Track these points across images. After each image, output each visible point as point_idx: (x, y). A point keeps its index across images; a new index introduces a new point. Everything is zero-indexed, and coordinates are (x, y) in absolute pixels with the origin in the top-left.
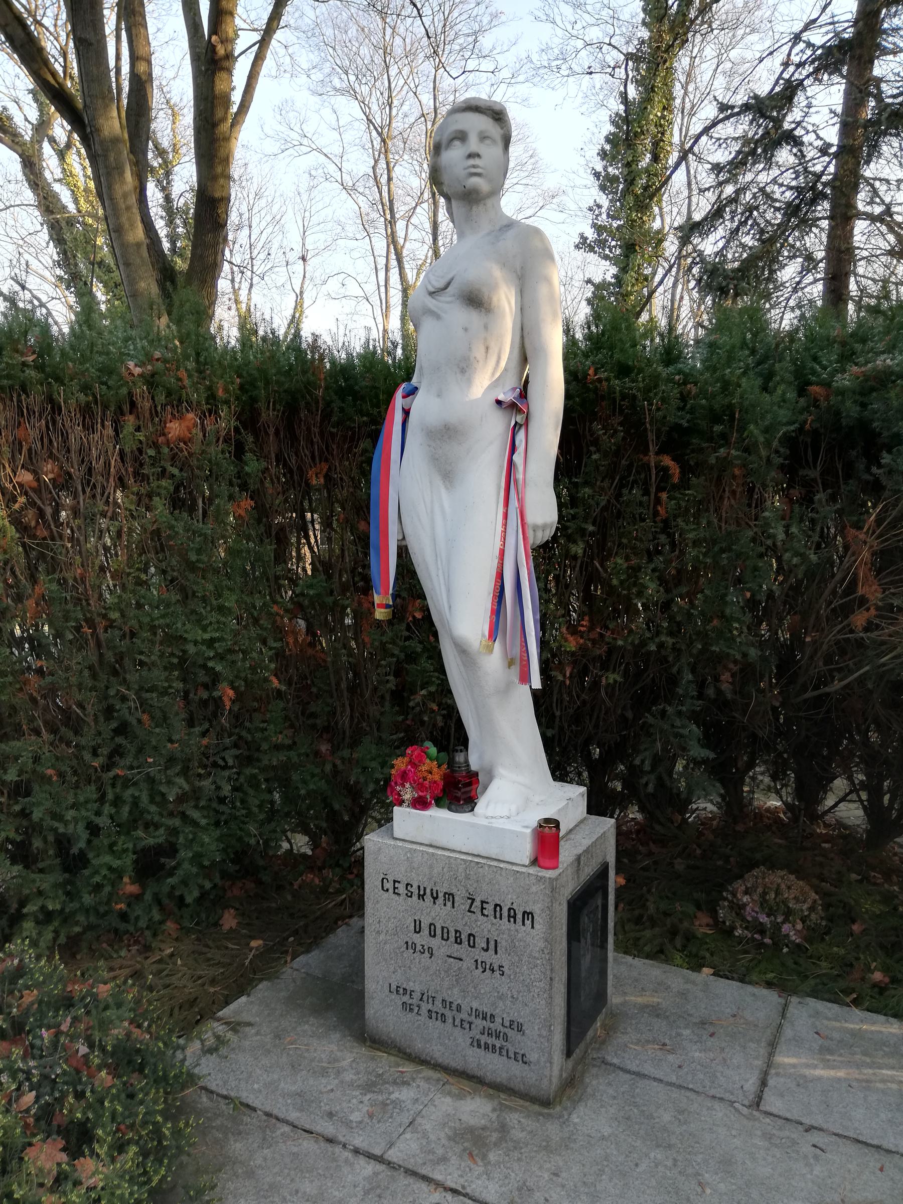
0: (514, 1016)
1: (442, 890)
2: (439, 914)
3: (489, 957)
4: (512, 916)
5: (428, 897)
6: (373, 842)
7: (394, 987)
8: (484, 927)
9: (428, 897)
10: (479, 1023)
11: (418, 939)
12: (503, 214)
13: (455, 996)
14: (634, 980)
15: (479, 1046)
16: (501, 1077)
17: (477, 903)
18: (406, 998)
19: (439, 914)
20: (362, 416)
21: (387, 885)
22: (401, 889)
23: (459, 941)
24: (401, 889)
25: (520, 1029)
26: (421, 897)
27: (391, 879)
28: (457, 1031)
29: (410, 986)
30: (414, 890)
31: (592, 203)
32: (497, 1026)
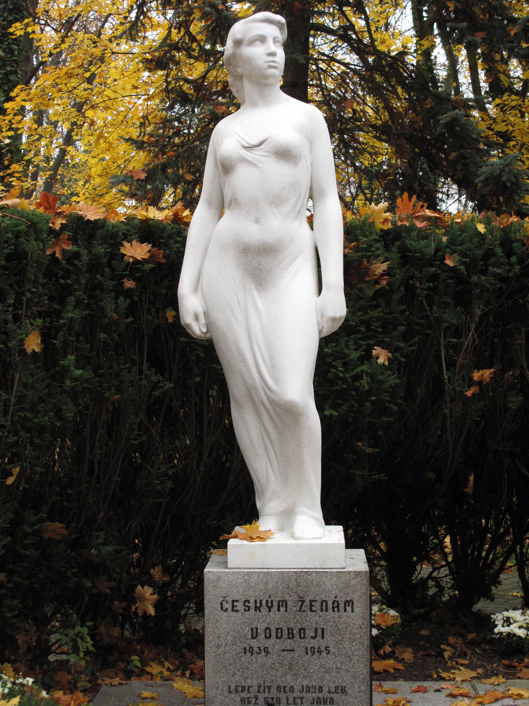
1: (341, 601)
4: (336, 606)
7: (233, 688)
8: (312, 620)
11: (254, 643)
13: (289, 681)
17: (307, 603)
18: (244, 694)
19: (275, 619)
21: (226, 606)
22: (240, 606)
24: (240, 606)
25: (343, 690)
27: (229, 599)
30: (252, 605)
32: (325, 694)
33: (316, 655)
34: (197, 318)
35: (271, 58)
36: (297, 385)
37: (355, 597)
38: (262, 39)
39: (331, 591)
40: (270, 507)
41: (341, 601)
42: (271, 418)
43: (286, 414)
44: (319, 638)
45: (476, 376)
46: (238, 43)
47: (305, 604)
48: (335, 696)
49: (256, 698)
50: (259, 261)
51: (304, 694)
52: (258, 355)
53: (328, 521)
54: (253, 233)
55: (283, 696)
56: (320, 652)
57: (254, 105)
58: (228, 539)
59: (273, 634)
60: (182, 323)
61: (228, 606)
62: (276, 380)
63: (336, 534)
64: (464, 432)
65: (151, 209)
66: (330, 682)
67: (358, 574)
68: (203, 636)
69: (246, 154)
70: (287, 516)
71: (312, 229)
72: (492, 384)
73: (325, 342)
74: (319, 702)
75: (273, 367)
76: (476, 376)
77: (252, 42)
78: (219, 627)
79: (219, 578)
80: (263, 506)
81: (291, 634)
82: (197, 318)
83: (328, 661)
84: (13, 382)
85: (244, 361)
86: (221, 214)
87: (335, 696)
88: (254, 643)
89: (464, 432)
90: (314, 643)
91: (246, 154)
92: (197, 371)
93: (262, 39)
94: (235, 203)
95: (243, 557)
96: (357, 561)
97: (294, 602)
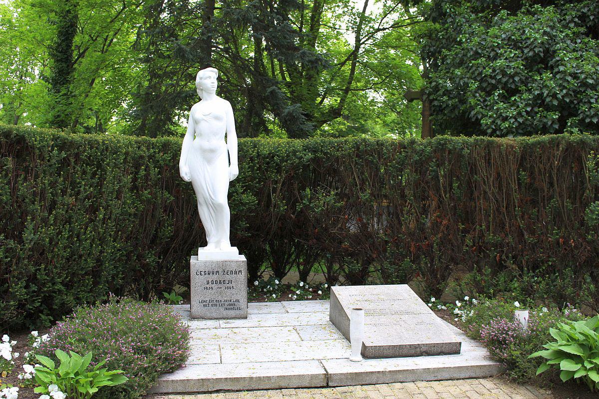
0: (237, 298)
1: (237, 271)
2: (215, 277)
4: (236, 273)
6: (193, 260)
7: (200, 301)
8: (228, 277)
9: (211, 274)
12: (182, 180)
13: (220, 298)
15: (227, 309)
16: (234, 315)
17: (226, 272)
18: (204, 304)
19: (215, 277)
21: (198, 273)
22: (203, 273)
24: (203, 273)
30: (207, 273)
32: (232, 302)
33: (229, 289)
34: (186, 174)
35: (213, 84)
36: (222, 198)
37: (242, 269)
38: (210, 77)
39: (234, 267)
40: (211, 239)
41: (237, 271)
42: (212, 208)
43: (216, 208)
44: (230, 283)
46: (201, 78)
49: (209, 304)
50: (208, 154)
51: (225, 303)
52: (209, 190)
53: (232, 245)
54: (206, 145)
55: (218, 304)
56: (230, 288)
57: (206, 100)
59: (214, 282)
60: (181, 176)
61: (199, 273)
62: (215, 196)
63: (235, 250)
64: (278, 217)
66: (234, 298)
67: (243, 261)
69: (204, 117)
70: (218, 243)
71: (226, 134)
73: (232, 184)
74: (598, 256)
75: (214, 191)
77: (206, 79)
78: (197, 282)
80: (209, 240)
81: (220, 282)
82: (186, 174)
83: (233, 291)
84: (121, 197)
85: (204, 189)
86: (194, 139)
88: (208, 286)
89: (278, 217)
90: (228, 285)
91: (204, 117)
92: (185, 196)
93: (210, 77)
94: (201, 135)
95: (205, 256)
96: (243, 258)
97: (220, 271)
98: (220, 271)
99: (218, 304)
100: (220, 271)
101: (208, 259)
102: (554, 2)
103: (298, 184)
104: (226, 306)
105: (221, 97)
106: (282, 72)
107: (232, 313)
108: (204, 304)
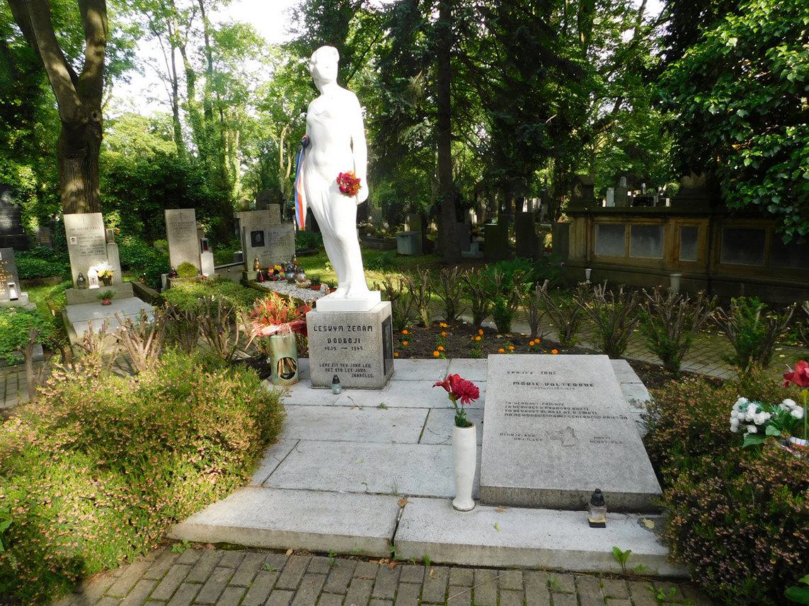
3: (357, 345)
5: (333, 330)
8: (353, 335)
9: (333, 330)
10: (355, 368)
11: (329, 345)
14: (399, 364)
16: (364, 384)
17: (351, 327)
18: (326, 367)
19: (338, 334)
20: (136, 262)
21: (316, 329)
22: (322, 329)
23: (345, 342)
24: (322, 329)
25: (369, 366)
26: (330, 330)
27: (317, 326)
28: (347, 373)
29: (328, 362)
31: (131, 81)
33: (360, 350)
45: (668, 200)
47: (351, 328)
48: (366, 368)
55: (343, 368)
58: (802, 407)
61: (317, 329)
65: (241, 185)
68: (122, 270)
72: (735, 199)
76: (668, 200)
79: (313, 317)
87: (366, 368)
98: (345, 326)
99: (343, 368)
100: (345, 326)
101: (333, 315)
102: (736, 4)
103: (763, 312)
104: (354, 372)
105: (347, 89)
106: (286, 165)
107: (361, 381)
108: (326, 367)
